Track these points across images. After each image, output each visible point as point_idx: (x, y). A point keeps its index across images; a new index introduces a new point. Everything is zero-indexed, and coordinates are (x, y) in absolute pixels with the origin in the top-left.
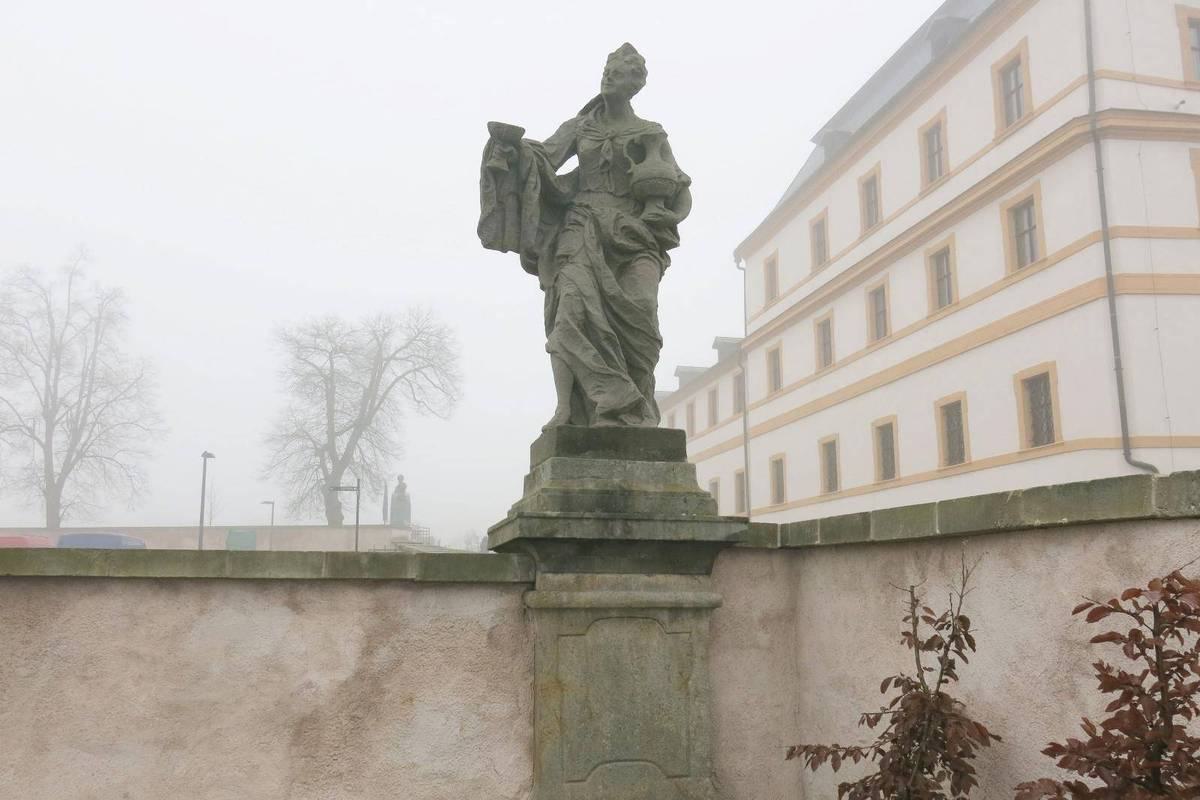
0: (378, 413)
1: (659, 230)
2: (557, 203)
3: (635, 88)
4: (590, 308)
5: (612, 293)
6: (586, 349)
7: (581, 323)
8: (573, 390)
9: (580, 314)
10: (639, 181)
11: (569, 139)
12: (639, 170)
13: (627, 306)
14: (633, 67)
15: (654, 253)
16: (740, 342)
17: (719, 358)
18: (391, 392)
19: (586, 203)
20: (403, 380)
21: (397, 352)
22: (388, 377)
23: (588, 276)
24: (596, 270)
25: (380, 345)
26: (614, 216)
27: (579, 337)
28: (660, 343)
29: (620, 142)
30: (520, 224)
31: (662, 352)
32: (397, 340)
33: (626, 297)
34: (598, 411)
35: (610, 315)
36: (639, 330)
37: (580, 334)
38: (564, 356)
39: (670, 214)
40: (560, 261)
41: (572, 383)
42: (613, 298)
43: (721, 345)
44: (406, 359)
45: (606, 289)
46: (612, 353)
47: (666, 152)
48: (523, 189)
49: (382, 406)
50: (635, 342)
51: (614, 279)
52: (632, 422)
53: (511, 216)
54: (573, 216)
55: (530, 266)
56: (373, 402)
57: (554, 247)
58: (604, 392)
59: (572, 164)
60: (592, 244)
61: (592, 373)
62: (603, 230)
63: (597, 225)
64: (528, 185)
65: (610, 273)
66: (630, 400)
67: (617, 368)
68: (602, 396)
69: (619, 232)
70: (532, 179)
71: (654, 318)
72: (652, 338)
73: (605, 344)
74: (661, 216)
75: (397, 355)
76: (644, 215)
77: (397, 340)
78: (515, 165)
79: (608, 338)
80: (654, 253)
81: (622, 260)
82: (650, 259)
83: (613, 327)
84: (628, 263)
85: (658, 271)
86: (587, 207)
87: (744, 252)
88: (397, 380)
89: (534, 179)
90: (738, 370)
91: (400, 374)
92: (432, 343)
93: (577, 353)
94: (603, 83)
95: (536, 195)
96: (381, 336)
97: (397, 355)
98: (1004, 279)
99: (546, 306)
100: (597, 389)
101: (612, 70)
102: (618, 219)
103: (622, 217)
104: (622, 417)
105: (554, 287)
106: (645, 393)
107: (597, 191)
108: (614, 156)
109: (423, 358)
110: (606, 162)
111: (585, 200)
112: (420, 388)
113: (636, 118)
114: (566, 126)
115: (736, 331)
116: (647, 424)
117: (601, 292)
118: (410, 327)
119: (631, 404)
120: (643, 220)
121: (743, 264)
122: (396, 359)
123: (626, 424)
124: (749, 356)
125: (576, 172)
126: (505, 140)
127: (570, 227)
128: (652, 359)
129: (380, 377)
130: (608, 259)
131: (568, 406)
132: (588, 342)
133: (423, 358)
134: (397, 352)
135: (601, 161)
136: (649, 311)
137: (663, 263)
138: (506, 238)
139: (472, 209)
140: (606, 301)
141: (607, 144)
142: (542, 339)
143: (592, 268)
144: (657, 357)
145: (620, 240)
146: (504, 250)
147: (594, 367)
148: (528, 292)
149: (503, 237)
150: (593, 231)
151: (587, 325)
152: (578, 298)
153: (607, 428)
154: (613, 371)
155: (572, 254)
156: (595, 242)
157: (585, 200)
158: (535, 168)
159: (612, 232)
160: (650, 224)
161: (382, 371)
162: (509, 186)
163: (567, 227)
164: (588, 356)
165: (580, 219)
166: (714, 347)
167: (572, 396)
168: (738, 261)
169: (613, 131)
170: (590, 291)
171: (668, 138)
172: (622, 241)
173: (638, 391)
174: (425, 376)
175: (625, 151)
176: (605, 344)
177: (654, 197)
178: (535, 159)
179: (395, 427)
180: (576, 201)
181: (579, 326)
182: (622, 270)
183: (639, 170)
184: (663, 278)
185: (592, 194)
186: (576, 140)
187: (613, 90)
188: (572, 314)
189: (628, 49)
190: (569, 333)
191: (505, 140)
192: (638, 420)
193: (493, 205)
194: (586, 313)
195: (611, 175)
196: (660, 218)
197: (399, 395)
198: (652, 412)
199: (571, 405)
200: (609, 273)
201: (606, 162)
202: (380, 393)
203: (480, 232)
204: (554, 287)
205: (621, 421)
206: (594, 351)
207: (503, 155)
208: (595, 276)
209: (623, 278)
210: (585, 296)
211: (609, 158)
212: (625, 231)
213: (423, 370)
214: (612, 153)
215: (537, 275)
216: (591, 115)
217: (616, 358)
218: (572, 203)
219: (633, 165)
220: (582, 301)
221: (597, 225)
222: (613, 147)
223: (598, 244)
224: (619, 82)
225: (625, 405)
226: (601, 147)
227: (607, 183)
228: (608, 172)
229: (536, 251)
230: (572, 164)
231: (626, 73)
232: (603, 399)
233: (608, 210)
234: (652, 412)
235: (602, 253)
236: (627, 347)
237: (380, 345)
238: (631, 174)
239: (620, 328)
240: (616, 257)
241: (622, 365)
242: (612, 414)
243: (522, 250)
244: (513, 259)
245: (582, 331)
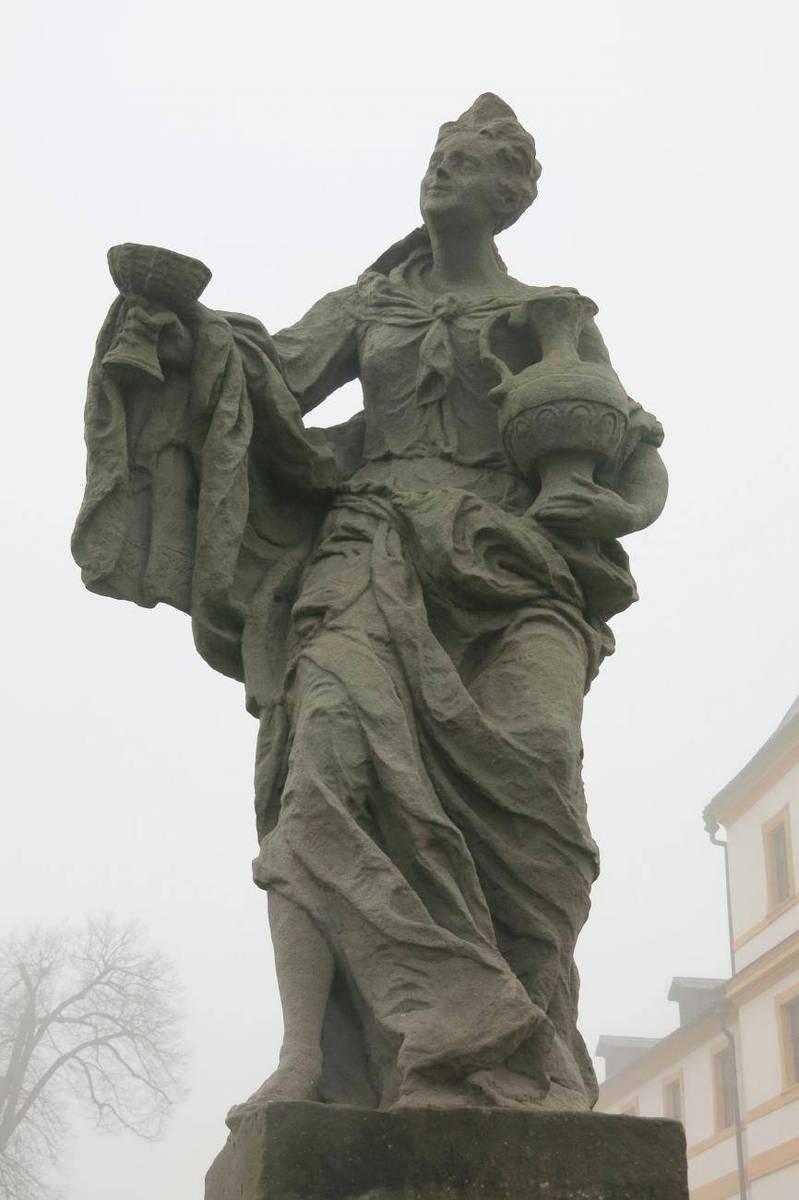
0: (21, 1127)
1: (577, 543)
2: (299, 492)
3: (507, 219)
4: (385, 753)
5: (450, 714)
6: (370, 871)
7: (359, 798)
8: (333, 1000)
9: (356, 769)
10: (521, 413)
11: (338, 343)
12: (522, 385)
13: (495, 754)
14: (502, 144)
15: (569, 609)
16: (723, 987)
17: (682, 1021)
18: (47, 1087)
19: (377, 483)
20: (72, 1061)
21: (63, 1005)
22: (43, 1056)
23: (377, 662)
24: (405, 653)
25: (31, 991)
26: (453, 504)
27: (352, 838)
28: (589, 858)
29: (466, 324)
30: (192, 531)
31: (597, 892)
32: (65, 982)
33: (490, 724)
34: (405, 1061)
35: (444, 782)
36: (524, 818)
37: (354, 826)
38: (306, 895)
39: (608, 498)
40: (304, 625)
41: (328, 976)
42: (453, 727)
43: (683, 992)
44: (81, 1021)
45: (431, 703)
46: (452, 886)
47: (591, 348)
48: (204, 434)
49: (30, 1111)
50: (518, 856)
51: (454, 676)
52: (511, 1095)
53: (169, 507)
54: (342, 518)
55: (222, 653)
56: (13, 1102)
57: (287, 595)
58: (425, 1005)
59: (343, 404)
60: (391, 579)
61: (390, 946)
62: (424, 542)
63: (407, 532)
64: (216, 422)
65: (441, 657)
66: (509, 1023)
67: (464, 930)
68: (419, 1015)
69: (469, 544)
70: (228, 405)
71: (572, 785)
72: (567, 844)
73: (429, 860)
74: (587, 502)
75: (64, 1013)
76: (543, 503)
77: (65, 982)
78: (180, 369)
79: (437, 844)
80: (569, 609)
81: (474, 625)
82: (561, 626)
83: (447, 809)
84: (497, 635)
85: (578, 659)
86: (382, 492)
87: (722, 811)
88: (59, 1062)
89: (232, 405)
90: (720, 1040)
91: (66, 1049)
92: (132, 989)
93: (344, 883)
94: (425, 187)
95: (239, 449)
96: (33, 976)
97: (64, 1013)
98: (782, 1095)
99: (260, 756)
100: (402, 996)
101: (447, 154)
102: (461, 515)
103: (478, 508)
104: (480, 1078)
105: (283, 702)
106: (552, 1010)
107: (409, 457)
108: (456, 363)
109: (112, 1019)
110: (435, 377)
111: (376, 477)
112: (105, 1077)
113: (513, 282)
114: (333, 301)
115: (715, 965)
116: (556, 1103)
117: (419, 713)
118: (89, 958)
119: (508, 1039)
120: (537, 518)
121: (722, 834)
122: (62, 1020)
123: (491, 1101)
124: (741, 1013)
125: (358, 424)
126: (156, 289)
127: (336, 547)
128: (570, 912)
129: (28, 1055)
130: (438, 619)
131: (316, 1046)
132: (379, 853)
133: (112, 1019)
134: (63, 1005)
135: (423, 373)
136: (559, 763)
137: (597, 650)
138: (153, 565)
139: (62, 477)
140: (434, 739)
141: (435, 332)
142: (247, 845)
143: (392, 644)
144: (586, 905)
145: (473, 568)
146: (148, 602)
147: (397, 925)
148: (221, 719)
149: (145, 563)
150: (397, 550)
151: (376, 805)
152: (349, 722)
153: (431, 1114)
154: (452, 938)
155: (337, 604)
156: (400, 573)
157: (376, 477)
158: (238, 378)
159: (449, 544)
160: (552, 525)
161: (32, 1042)
162: (165, 425)
163: (326, 546)
164: (376, 892)
165: (361, 523)
166: (672, 996)
167: (327, 1018)
168: (712, 828)
169: (452, 300)
170: (386, 703)
171: (598, 320)
172: (476, 571)
173: (526, 999)
174: (116, 1052)
175: (483, 342)
176: (429, 860)
177: (564, 455)
178: (239, 355)
179: (52, 1156)
180: (354, 484)
181: (350, 803)
182: (478, 655)
183: (522, 385)
184: (594, 683)
185: (395, 463)
186: (354, 333)
187: (451, 200)
188: (331, 769)
189: (490, 108)
190: (320, 822)
191: (156, 289)
192: (536, 1093)
193: (117, 473)
194: (371, 765)
195: (447, 414)
196: (585, 511)
197: (64, 1091)
198: (572, 1066)
199: (324, 1040)
200: (439, 667)
201: (435, 377)
202: (28, 1087)
203: (79, 547)
204: (283, 702)
205: (478, 1091)
206: (395, 878)
207: (146, 333)
208: (401, 664)
209: (481, 678)
210: (367, 715)
211: (442, 364)
212: (485, 544)
213: (112, 1043)
214: (448, 351)
215: (240, 677)
216: (395, 275)
217: (460, 900)
218: (346, 491)
219: (507, 374)
220: (363, 733)
221: (407, 532)
222: (451, 340)
223: (409, 584)
224: (465, 180)
225: (488, 1040)
226: (416, 344)
227: (435, 433)
228: (440, 402)
229: (236, 603)
230: (343, 404)
231: (485, 170)
232: (420, 1022)
233: (438, 495)
234: (572, 1066)
235: (420, 604)
236: (494, 872)
237: (31, 991)
238: (500, 398)
239: (472, 815)
240: (460, 617)
241: (481, 921)
242: (448, 1071)
243: (198, 601)
244: (173, 626)
245: (360, 819)
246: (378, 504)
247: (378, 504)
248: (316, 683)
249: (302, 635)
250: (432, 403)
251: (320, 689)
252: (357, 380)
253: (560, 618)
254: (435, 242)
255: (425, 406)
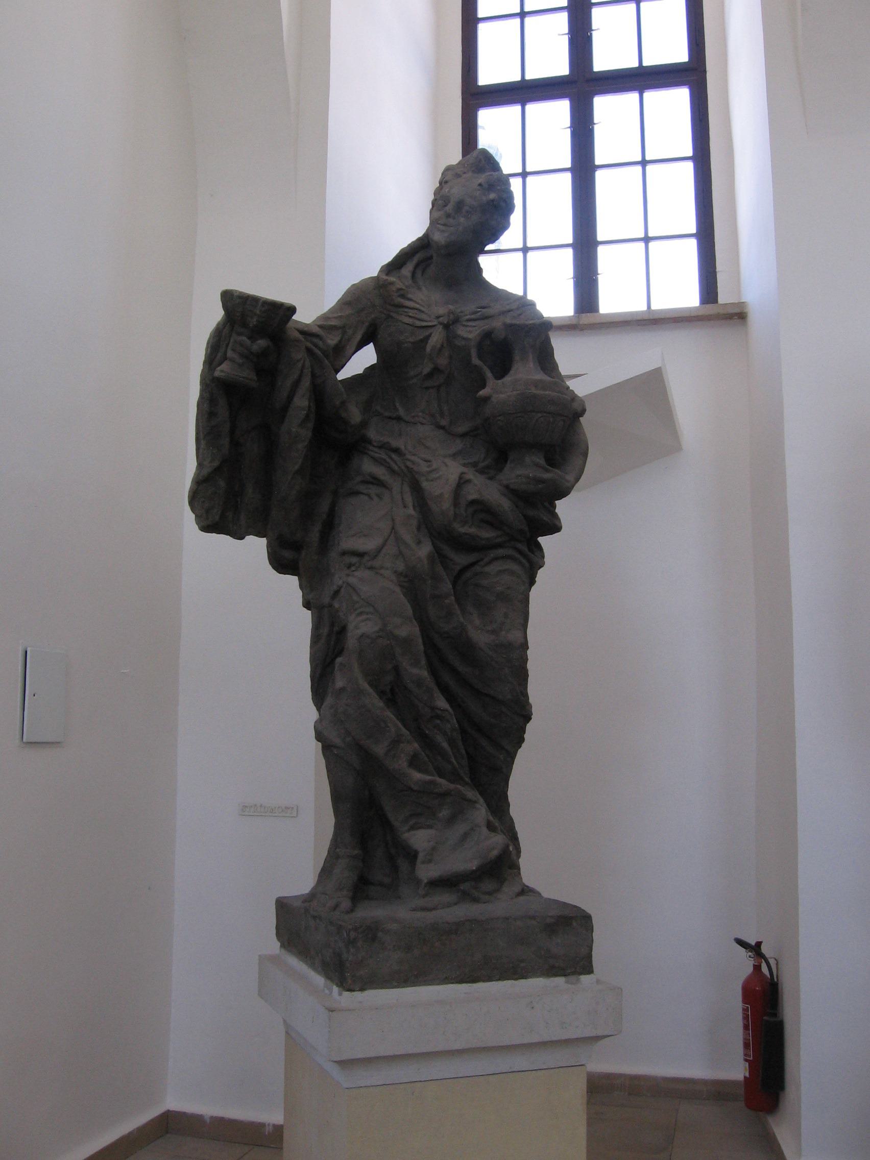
12: (501, 391)
15: (519, 546)
54: (368, 467)
80: (519, 546)
126: (282, 906)
175: (474, 353)
201: (436, 370)
211: (443, 361)
230: (364, 359)
246: (391, 458)
247: (391, 458)
248: (361, 610)
249: (349, 566)
250: (433, 387)
251: (364, 617)
252: (372, 344)
253: (518, 556)
254: (772, 1019)
255: (427, 388)
